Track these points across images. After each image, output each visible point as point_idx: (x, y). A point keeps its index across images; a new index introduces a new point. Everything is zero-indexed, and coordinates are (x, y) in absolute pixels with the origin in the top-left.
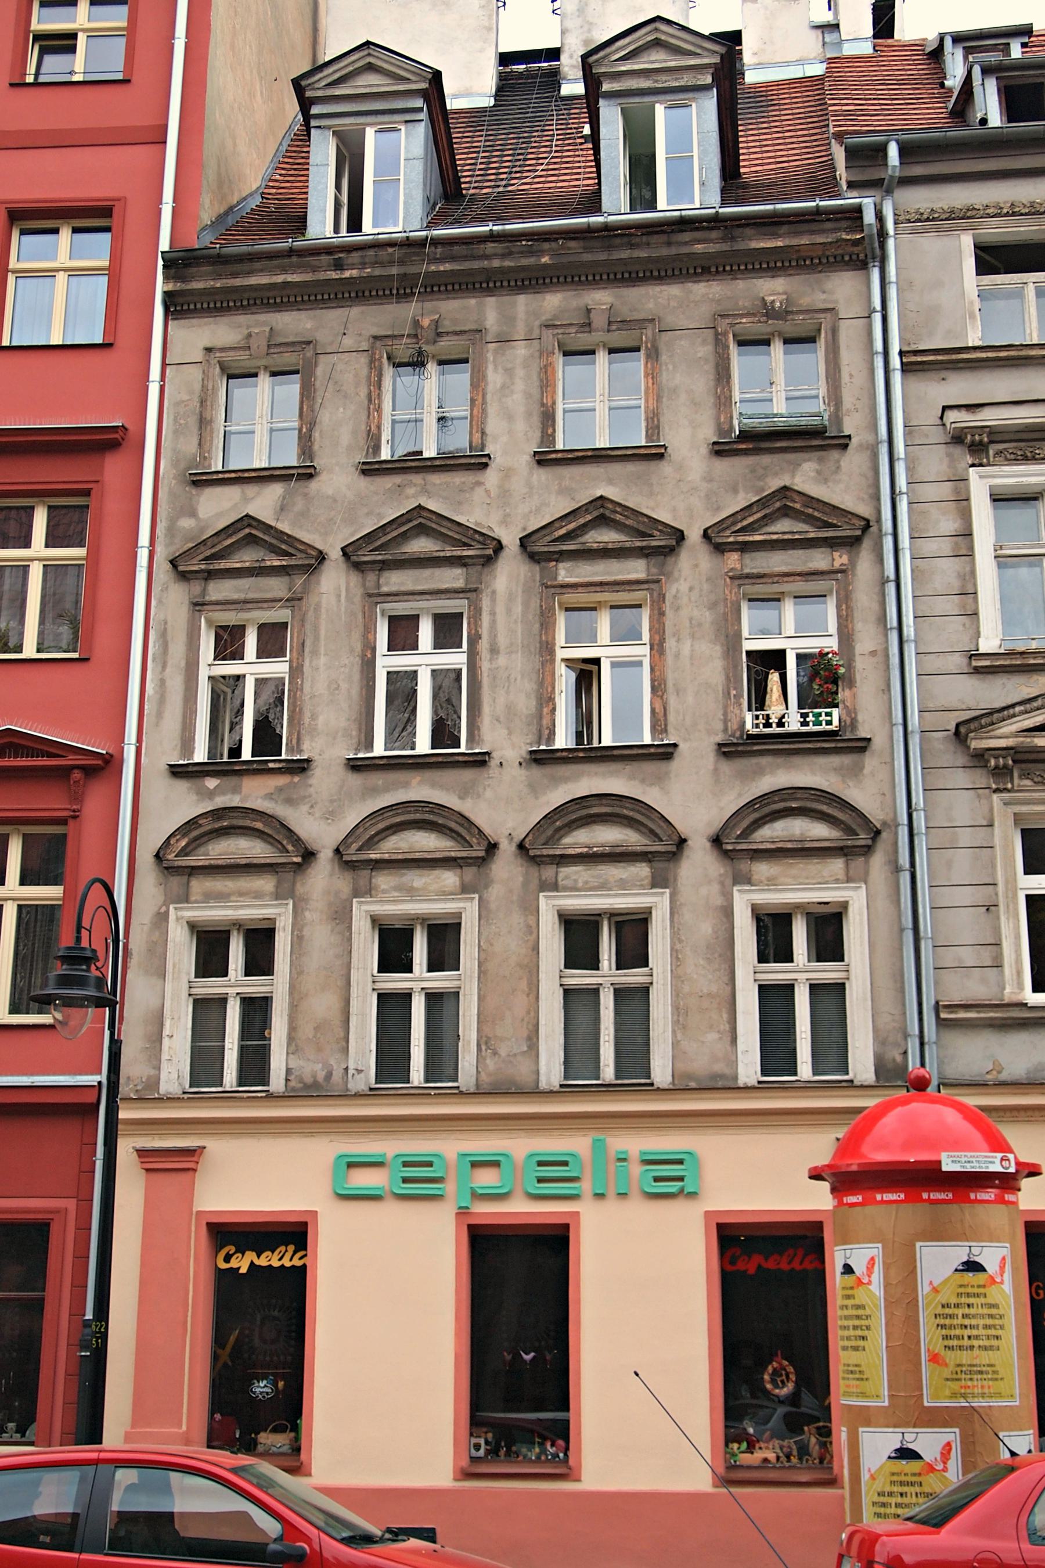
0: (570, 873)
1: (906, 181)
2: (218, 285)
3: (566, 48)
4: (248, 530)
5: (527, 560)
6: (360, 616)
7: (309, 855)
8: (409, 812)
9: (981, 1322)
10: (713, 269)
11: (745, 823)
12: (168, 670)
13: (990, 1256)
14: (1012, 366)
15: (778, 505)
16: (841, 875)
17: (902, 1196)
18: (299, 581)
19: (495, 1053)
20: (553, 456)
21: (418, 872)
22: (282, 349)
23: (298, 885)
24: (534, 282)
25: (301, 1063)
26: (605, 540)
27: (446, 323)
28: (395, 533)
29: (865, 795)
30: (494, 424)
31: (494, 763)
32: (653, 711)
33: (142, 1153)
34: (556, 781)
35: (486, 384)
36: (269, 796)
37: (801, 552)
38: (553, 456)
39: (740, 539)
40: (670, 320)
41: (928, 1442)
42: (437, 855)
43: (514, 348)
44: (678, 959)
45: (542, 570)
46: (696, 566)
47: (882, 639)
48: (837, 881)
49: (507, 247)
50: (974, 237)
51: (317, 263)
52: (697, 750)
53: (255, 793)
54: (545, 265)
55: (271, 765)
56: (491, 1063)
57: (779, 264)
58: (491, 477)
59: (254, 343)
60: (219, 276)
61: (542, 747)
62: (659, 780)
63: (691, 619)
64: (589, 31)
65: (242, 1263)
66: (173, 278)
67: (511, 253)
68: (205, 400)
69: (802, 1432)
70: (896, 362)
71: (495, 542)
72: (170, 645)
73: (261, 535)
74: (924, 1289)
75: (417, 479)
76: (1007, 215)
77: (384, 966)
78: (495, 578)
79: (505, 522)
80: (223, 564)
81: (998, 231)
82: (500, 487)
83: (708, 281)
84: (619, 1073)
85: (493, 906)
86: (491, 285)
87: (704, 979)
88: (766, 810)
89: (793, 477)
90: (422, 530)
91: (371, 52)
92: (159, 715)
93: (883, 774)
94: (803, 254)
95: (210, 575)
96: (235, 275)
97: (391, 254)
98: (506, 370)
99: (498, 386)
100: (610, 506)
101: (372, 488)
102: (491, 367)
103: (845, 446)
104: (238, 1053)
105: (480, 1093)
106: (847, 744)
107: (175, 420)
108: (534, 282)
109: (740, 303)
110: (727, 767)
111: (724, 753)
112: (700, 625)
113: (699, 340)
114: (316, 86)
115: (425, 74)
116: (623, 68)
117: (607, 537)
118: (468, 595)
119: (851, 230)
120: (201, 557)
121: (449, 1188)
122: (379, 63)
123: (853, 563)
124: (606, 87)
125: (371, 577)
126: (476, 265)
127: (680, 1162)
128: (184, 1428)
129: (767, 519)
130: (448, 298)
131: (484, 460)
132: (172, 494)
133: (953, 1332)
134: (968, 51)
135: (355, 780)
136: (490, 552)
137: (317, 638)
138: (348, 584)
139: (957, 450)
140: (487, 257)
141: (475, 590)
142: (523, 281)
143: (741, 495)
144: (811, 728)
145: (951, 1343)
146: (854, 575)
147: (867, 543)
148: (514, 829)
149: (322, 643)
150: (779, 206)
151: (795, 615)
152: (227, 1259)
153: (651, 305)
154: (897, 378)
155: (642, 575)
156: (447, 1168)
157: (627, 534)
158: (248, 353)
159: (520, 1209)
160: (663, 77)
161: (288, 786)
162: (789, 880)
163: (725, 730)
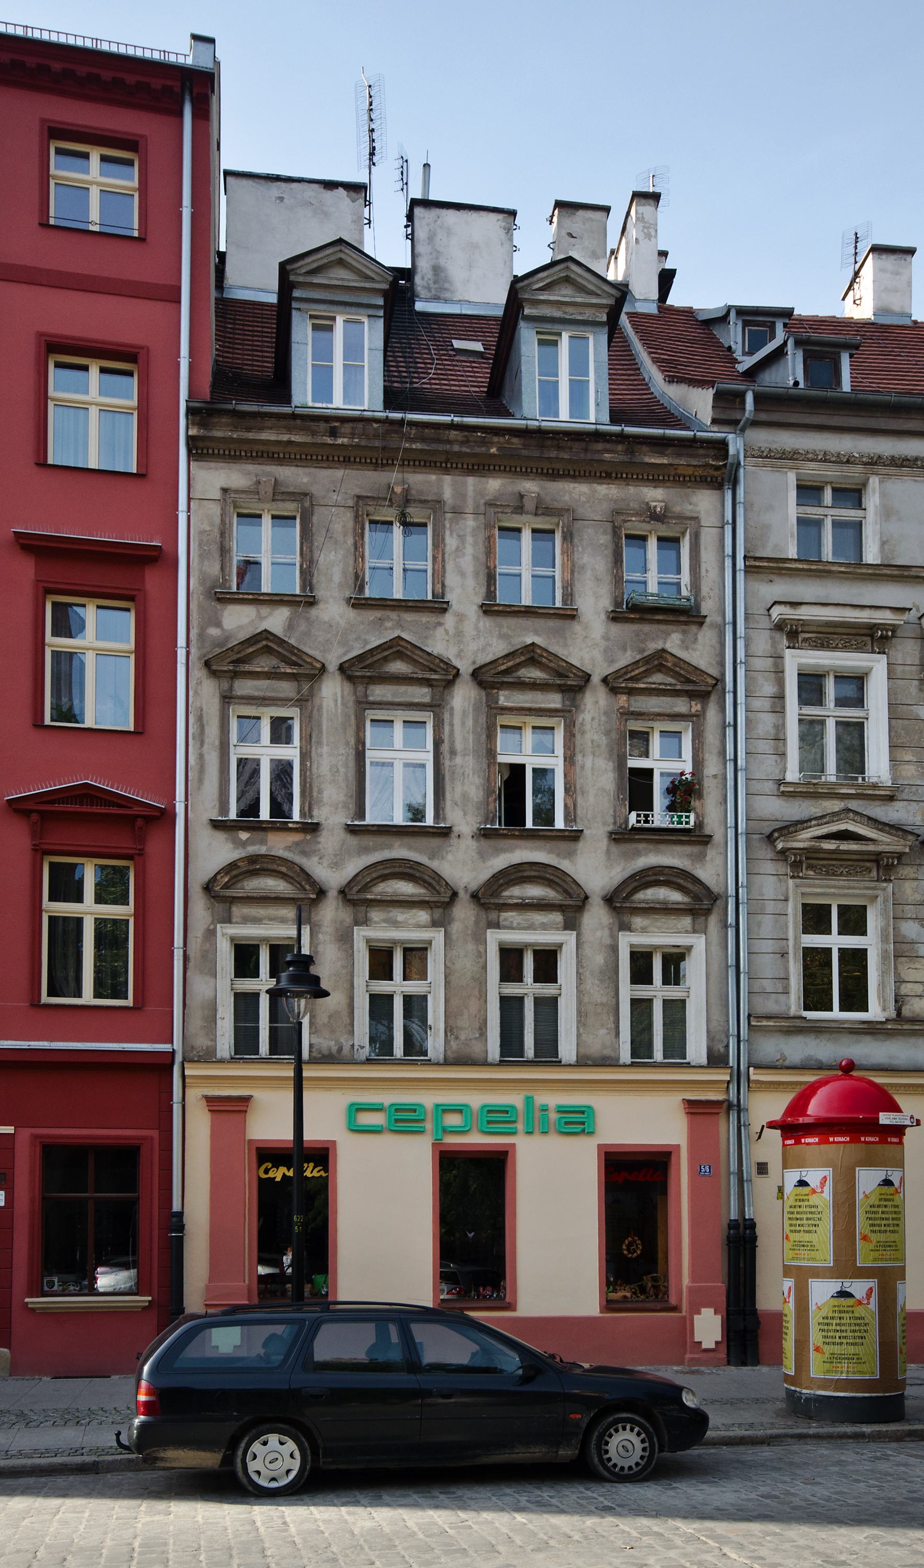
0: (508, 916)
1: (755, 424)
2: (235, 436)
3: (419, 270)
4: (264, 642)
5: (476, 686)
6: (353, 717)
7: (321, 893)
8: (394, 867)
9: (805, 1216)
10: (614, 475)
11: (628, 889)
12: (206, 746)
13: (814, 1176)
14: (817, 576)
15: (656, 662)
16: (689, 928)
17: (848, 1139)
18: (306, 687)
19: (457, 1038)
20: (496, 608)
21: (400, 910)
22: (284, 497)
23: (313, 914)
24: (481, 467)
25: (321, 1040)
26: (393, 671)
27: (413, 492)
28: (379, 656)
29: (707, 873)
30: (452, 579)
31: (453, 835)
32: (566, 806)
33: (209, 1100)
34: (498, 851)
35: (445, 545)
36: (288, 848)
37: (669, 699)
38: (496, 608)
39: (630, 685)
40: (581, 511)
41: (859, 1288)
42: (415, 899)
43: (465, 519)
44: (581, 979)
45: (487, 695)
46: (597, 702)
47: (721, 766)
48: (687, 932)
49: (466, 436)
50: (797, 474)
51: (316, 428)
52: (596, 834)
53: (278, 845)
54: (493, 455)
55: (290, 825)
56: (454, 1044)
57: (661, 478)
58: (449, 620)
59: (262, 488)
60: (236, 428)
61: (488, 826)
62: (570, 855)
63: (592, 741)
64: (437, 258)
65: (278, 1174)
66: (197, 424)
67: (468, 441)
68: (224, 533)
69: (643, 1280)
70: (740, 564)
71: (455, 671)
72: (206, 727)
73: (276, 647)
74: (860, 1196)
75: (393, 615)
76: (821, 461)
77: (373, 976)
78: (453, 698)
79: (459, 655)
80: (247, 668)
81: (813, 470)
82: (456, 628)
83: (609, 484)
84: (536, 1054)
85: (454, 937)
86: (449, 465)
87: (597, 993)
88: (644, 880)
89: (665, 643)
90: (400, 656)
91: (343, 248)
92: (201, 781)
93: (719, 860)
94: (679, 472)
95: (235, 675)
96: (249, 429)
97: (375, 429)
98: (459, 536)
99: (454, 548)
100: (539, 651)
101: (359, 619)
102: (448, 533)
103: (701, 624)
104: (276, 1031)
105: (448, 1062)
106: (697, 838)
107: (200, 545)
108: (481, 467)
109: (631, 505)
110: (615, 849)
111: (614, 839)
112: (599, 746)
113: (601, 530)
114: (298, 271)
115: (387, 276)
116: (542, 298)
117: (535, 674)
118: (433, 709)
119: (716, 458)
120: (229, 660)
121: (428, 1126)
122: (349, 260)
123: (704, 710)
124: (527, 311)
125: (361, 688)
126: (441, 447)
127: (583, 1113)
128: (247, 1282)
129: (648, 673)
130: (415, 472)
131: (445, 606)
132: (200, 606)
133: (876, 1222)
134: (746, 324)
135: (353, 841)
136: (451, 677)
137: (321, 732)
138: (342, 691)
139: (777, 635)
140: (449, 442)
141: (439, 706)
142: (473, 465)
143: (629, 653)
144: (642, 825)
145: (875, 1228)
146: (704, 719)
147: (713, 698)
148: (468, 883)
149: (325, 735)
150: (465, 419)
151: (533, 738)
152: (266, 1171)
153: (567, 498)
154: (740, 576)
155: (558, 706)
156: (425, 1114)
157: (549, 674)
158: (257, 497)
159: (476, 1139)
160: (570, 310)
161: (302, 841)
162: (656, 930)
163: (615, 823)
